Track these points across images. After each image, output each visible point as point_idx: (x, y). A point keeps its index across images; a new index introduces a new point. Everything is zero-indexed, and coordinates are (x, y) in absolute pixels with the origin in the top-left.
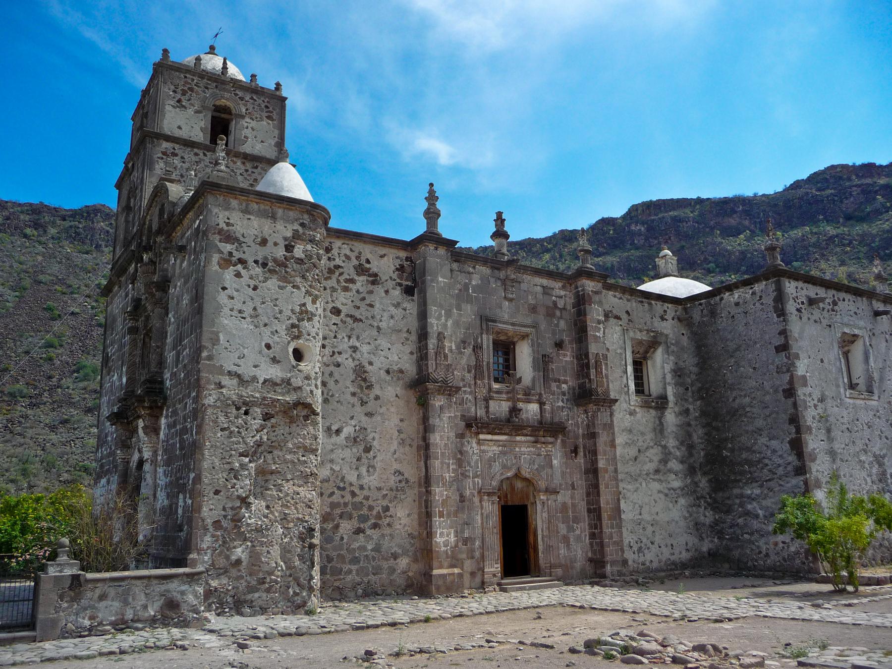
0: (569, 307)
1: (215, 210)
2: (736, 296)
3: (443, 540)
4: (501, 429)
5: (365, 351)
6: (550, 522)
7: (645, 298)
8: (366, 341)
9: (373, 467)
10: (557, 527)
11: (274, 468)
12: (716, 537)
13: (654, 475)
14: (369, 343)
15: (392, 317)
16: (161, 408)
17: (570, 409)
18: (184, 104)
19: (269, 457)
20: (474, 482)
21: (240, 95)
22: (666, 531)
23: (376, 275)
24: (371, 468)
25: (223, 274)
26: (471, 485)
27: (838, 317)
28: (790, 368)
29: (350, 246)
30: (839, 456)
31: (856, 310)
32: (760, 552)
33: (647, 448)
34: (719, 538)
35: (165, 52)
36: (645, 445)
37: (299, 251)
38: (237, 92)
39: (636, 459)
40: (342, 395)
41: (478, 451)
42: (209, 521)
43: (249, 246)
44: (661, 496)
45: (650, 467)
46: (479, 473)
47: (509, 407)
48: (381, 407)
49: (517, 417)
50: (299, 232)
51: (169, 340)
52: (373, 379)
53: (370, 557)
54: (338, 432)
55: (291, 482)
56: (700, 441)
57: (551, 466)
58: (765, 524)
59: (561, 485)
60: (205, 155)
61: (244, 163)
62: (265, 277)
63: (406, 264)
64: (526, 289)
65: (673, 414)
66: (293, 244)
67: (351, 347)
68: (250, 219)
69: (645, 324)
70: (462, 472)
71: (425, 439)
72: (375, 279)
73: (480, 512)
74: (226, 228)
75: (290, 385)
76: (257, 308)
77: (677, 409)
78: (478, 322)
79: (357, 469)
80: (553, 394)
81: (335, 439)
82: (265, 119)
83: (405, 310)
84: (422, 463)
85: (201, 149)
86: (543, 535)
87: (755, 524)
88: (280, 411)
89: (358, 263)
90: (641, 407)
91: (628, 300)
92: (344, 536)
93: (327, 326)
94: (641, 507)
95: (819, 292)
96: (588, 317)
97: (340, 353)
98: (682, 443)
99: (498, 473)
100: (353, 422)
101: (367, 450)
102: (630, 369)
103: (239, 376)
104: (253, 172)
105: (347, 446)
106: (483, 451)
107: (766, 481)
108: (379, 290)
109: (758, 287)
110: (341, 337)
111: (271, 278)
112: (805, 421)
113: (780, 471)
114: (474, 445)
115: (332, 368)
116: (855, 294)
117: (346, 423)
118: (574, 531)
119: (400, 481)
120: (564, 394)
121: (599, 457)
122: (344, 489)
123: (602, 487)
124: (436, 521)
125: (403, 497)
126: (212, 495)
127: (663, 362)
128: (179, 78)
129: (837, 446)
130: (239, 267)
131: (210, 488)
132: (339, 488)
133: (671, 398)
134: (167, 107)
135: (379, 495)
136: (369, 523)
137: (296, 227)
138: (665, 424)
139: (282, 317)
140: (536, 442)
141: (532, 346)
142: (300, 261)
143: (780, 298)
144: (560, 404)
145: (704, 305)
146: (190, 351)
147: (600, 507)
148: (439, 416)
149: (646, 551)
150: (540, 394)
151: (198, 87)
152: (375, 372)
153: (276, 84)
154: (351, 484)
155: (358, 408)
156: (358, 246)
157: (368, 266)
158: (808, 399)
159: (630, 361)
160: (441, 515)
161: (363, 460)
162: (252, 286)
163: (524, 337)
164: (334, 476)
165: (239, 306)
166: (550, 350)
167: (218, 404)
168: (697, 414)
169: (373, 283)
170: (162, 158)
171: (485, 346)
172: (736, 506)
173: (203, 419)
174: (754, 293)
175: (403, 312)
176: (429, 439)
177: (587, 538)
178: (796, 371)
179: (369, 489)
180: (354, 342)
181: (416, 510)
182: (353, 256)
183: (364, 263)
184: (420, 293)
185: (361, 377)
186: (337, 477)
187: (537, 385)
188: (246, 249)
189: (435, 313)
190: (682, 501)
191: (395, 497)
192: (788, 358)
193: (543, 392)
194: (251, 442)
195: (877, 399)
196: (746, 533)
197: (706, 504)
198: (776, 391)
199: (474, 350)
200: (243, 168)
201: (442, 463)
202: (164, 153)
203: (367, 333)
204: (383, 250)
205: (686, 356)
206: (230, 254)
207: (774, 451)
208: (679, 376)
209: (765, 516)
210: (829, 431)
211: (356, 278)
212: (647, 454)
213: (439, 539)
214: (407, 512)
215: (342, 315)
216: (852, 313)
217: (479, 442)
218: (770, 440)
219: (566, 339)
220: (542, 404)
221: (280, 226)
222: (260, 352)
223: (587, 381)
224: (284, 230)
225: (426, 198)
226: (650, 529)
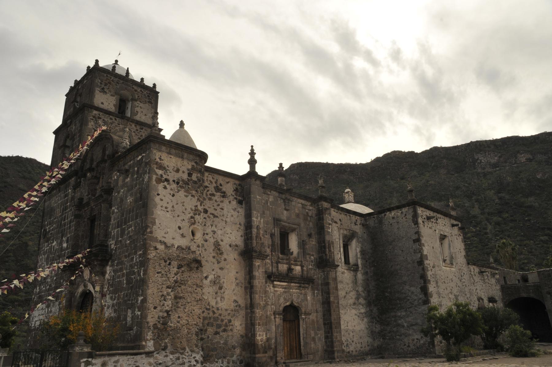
0: (314, 215)
1: (155, 151)
2: (393, 214)
5: (219, 234)
6: (306, 330)
7: (348, 213)
8: (220, 228)
9: (223, 298)
10: (310, 333)
11: (182, 295)
12: (382, 338)
13: (353, 306)
15: (232, 216)
16: (108, 261)
17: (314, 269)
18: (105, 90)
19: (179, 289)
20: (271, 307)
21: (135, 89)
22: (359, 335)
24: (222, 298)
25: (158, 187)
26: (270, 309)
27: (438, 226)
28: (420, 251)
29: (212, 176)
30: (442, 295)
31: (445, 223)
32: (405, 345)
33: (350, 292)
34: (383, 339)
35: (97, 61)
36: (349, 290)
37: (194, 177)
38: (134, 87)
39: (345, 297)
40: (208, 257)
41: (273, 291)
42: (151, 324)
43: (171, 172)
44: (357, 317)
45: (351, 301)
46: (273, 303)
47: (287, 268)
49: (291, 273)
50: (194, 166)
51: (112, 222)
52: (223, 249)
53: (222, 347)
55: (190, 304)
56: (373, 288)
57: (307, 300)
58: (408, 330)
59: (311, 310)
60: (116, 120)
61: (136, 126)
63: (239, 187)
65: (361, 274)
66: (191, 172)
67: (213, 231)
68: (171, 157)
71: (250, 283)
72: (224, 195)
73: (274, 324)
74: (159, 161)
76: (174, 206)
78: (273, 221)
79: (216, 298)
80: (307, 262)
82: (147, 103)
83: (238, 212)
84: (248, 296)
85: (114, 116)
86: (303, 338)
87: (402, 330)
88: (186, 264)
89: (216, 185)
90: (347, 270)
91: (340, 214)
94: (348, 322)
95: (431, 213)
96: (325, 221)
98: (365, 289)
99: (283, 303)
100: (214, 273)
101: (221, 288)
102: (342, 250)
104: (140, 131)
105: (211, 286)
106: (276, 291)
107: (408, 308)
108: (226, 201)
109: (404, 210)
110: (208, 225)
111: (181, 190)
112: (428, 277)
113: (416, 303)
114: (271, 287)
116: (444, 215)
117: (210, 273)
118: (318, 335)
119: (236, 306)
120: (312, 262)
121: (331, 295)
123: (332, 311)
124: (257, 328)
125: (238, 315)
126: (152, 309)
127: (356, 247)
128: (103, 76)
129: (441, 291)
130: (166, 183)
131: (151, 305)
133: (360, 265)
134: (96, 91)
136: (222, 329)
137: (194, 164)
138: (357, 279)
139: (187, 212)
140: (300, 287)
141: (298, 235)
142: (195, 182)
143: (415, 216)
144: (311, 267)
145: (376, 218)
146: (135, 229)
147: (331, 323)
148: (258, 270)
149: (350, 346)
150: (301, 261)
151: (114, 82)
152: (224, 245)
153: (153, 84)
154: (213, 307)
155: (216, 265)
156: (216, 176)
157: (221, 187)
158: (428, 266)
159: (342, 245)
160: (259, 325)
161: (218, 294)
162: (172, 194)
163: (293, 230)
164: (204, 302)
165: (165, 205)
166: (305, 238)
167: (155, 258)
168: (372, 274)
170: (93, 119)
171: (276, 234)
172: (392, 322)
173: (148, 266)
174: (402, 213)
175: (238, 213)
176: (253, 283)
177: (324, 338)
178: (423, 252)
180: (214, 228)
181: (244, 322)
182: (213, 181)
183: (219, 186)
184: (246, 204)
185: (217, 248)
186: (206, 302)
187: (300, 256)
188: (169, 174)
189: (255, 215)
190: (365, 320)
191: (234, 315)
192: (420, 245)
193: (303, 260)
194: (172, 280)
195: (454, 267)
196: (398, 335)
197: (376, 321)
198: (414, 262)
199: (271, 236)
200: (135, 128)
201: (259, 296)
202: (94, 117)
203: (220, 224)
204: (228, 180)
205: (366, 244)
206: (162, 176)
207: (413, 293)
208: (363, 254)
209: (408, 326)
210: (437, 283)
211: (215, 193)
212: (350, 295)
213: (259, 338)
214: (240, 323)
215: (209, 213)
216: (443, 225)
217: (274, 287)
218: (410, 287)
219: (313, 232)
220: (302, 267)
221: (185, 162)
222: (175, 231)
223: (324, 255)
225: (249, 153)
226: (352, 334)
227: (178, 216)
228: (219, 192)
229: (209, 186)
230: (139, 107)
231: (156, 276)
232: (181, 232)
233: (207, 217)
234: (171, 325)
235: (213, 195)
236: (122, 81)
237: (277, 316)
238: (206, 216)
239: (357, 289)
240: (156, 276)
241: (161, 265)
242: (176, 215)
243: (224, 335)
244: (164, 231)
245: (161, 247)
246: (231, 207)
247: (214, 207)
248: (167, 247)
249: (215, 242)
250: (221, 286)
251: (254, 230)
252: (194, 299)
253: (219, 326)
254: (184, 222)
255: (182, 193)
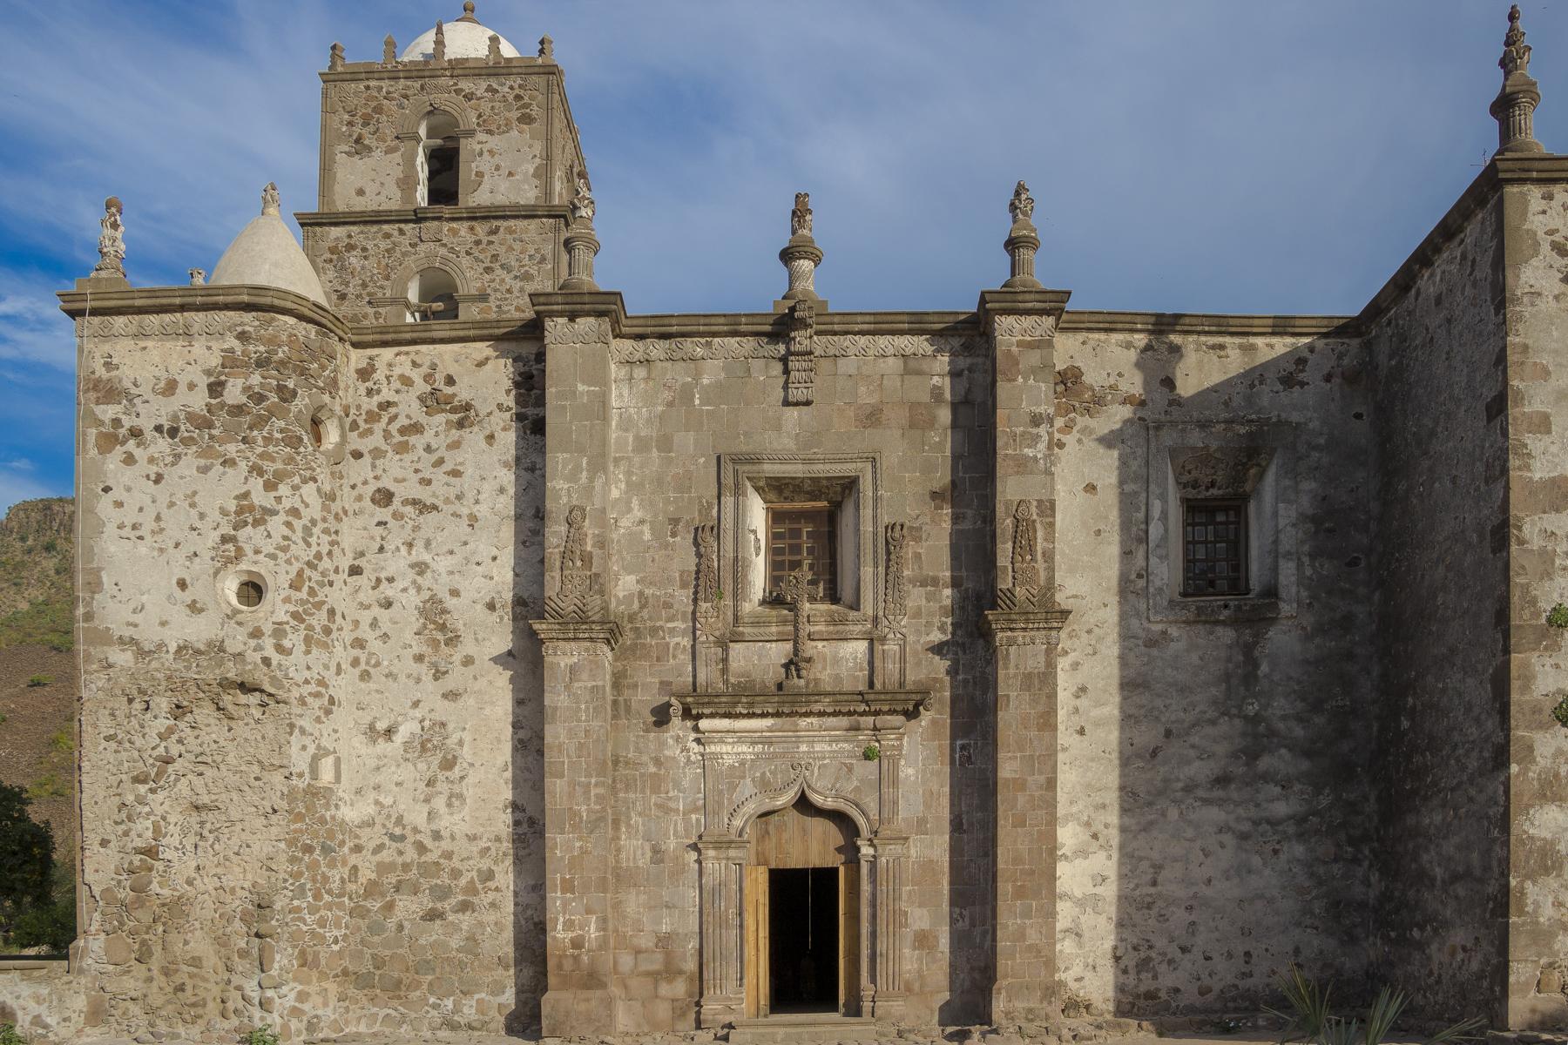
3: (570, 935)
4: (751, 705)
5: (443, 570)
8: (445, 549)
9: (460, 796)
14: (451, 552)
20: (687, 821)
23: (467, 407)
26: (680, 828)
37: (234, 393)
38: (461, 85)
39: (1154, 754)
44: (1228, 838)
48: (475, 678)
49: (799, 677)
52: (460, 625)
54: (389, 733)
62: (175, 455)
64: (853, 371)
67: (412, 566)
68: (145, 348)
69: (1226, 404)
70: (659, 801)
72: (464, 416)
75: (224, 651)
77: (1308, 620)
79: (427, 801)
81: (382, 745)
92: (406, 924)
93: (365, 529)
94: (1158, 868)
97: (391, 580)
100: (418, 713)
101: (448, 764)
103: (133, 641)
108: (474, 437)
110: (393, 547)
115: (376, 611)
122: (402, 838)
130: (131, 445)
132: (393, 837)
135: (475, 848)
136: (453, 901)
142: (238, 410)
154: (416, 830)
157: (448, 390)
160: (568, 887)
162: (153, 477)
169: (461, 425)
170: (331, 261)
179: (453, 838)
182: (416, 376)
183: (442, 386)
185: (435, 622)
186: (389, 816)
200: (471, 238)
201: (573, 784)
206: (117, 422)
215: (396, 502)
224: (205, 352)
227: (177, 545)
228: (443, 411)
229: (395, 398)
230: (486, 154)
231: (101, 748)
232: (188, 596)
233: (389, 518)
234: (158, 890)
235: (416, 428)
236: (417, 85)
237: (711, 853)
238: (384, 514)
239: (1251, 709)
240: (101, 748)
241: (117, 713)
242: (171, 544)
243: (466, 920)
244: (132, 605)
245: (122, 658)
246: (495, 458)
247: (420, 475)
248: (142, 653)
249: (424, 602)
250: (450, 757)
251: (556, 528)
252: (254, 809)
253: (442, 893)
254: (197, 560)
255: (190, 462)
